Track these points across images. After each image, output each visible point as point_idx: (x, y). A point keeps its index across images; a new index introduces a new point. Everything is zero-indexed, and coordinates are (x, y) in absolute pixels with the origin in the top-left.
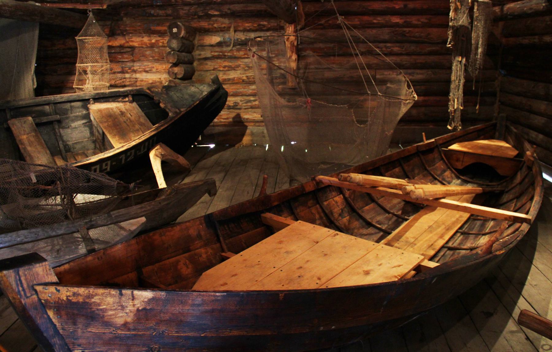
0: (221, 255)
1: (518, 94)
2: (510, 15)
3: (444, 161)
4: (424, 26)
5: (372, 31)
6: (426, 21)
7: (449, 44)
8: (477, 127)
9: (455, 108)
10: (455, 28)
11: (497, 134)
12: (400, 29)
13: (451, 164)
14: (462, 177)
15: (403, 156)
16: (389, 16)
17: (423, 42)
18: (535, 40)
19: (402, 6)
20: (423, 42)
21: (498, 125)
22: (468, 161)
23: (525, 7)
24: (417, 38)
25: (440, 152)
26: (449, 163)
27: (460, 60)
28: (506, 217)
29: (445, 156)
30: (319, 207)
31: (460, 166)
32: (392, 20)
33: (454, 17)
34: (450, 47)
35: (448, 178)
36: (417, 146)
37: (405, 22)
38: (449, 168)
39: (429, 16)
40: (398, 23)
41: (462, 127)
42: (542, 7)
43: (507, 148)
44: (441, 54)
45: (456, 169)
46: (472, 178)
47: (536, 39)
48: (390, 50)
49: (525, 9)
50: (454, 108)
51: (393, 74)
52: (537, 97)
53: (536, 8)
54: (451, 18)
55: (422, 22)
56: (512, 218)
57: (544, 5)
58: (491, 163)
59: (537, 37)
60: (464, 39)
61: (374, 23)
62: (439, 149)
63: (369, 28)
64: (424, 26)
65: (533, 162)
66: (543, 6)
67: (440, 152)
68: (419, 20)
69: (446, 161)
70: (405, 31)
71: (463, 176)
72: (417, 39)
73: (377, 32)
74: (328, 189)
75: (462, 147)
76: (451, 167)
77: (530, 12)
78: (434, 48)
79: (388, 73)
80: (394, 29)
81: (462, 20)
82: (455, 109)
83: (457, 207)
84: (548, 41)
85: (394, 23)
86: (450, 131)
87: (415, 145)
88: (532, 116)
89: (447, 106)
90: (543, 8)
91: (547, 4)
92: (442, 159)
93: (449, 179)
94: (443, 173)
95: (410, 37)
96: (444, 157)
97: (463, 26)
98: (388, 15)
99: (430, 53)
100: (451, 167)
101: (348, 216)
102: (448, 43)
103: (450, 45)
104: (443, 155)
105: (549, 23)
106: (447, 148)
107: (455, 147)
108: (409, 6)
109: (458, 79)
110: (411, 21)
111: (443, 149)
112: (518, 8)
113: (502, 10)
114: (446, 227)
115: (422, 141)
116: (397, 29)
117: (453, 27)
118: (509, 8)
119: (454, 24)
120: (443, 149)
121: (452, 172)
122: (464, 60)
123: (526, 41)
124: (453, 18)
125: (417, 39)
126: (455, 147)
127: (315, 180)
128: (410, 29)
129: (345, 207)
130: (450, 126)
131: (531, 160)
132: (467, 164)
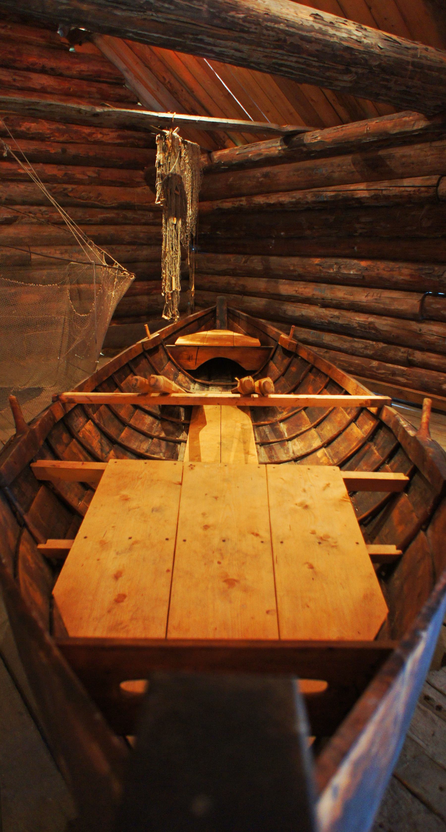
0: (40, 550)
1: (224, 273)
2: (224, 165)
3: (173, 362)
4: (92, 182)
5: (18, 187)
6: (94, 175)
7: (159, 200)
8: (198, 315)
9: (174, 289)
10: (166, 177)
11: (218, 322)
12: (60, 186)
13: (181, 366)
14: (200, 381)
15: (131, 359)
16: (41, 164)
17: (93, 206)
18: (241, 203)
19: (60, 150)
20: (93, 206)
21: (218, 311)
22: (204, 358)
23: (249, 152)
24: (84, 200)
25: (165, 350)
26: (179, 364)
27: (175, 223)
28: (362, 402)
29: (172, 354)
30: (76, 443)
31: (193, 366)
32: (46, 171)
33: (163, 161)
34: (159, 204)
35: (184, 383)
36: (142, 343)
37: (66, 174)
38: (180, 370)
39: (97, 169)
40: (55, 176)
41: (180, 316)
42: (277, 152)
43: (241, 336)
44: (116, 224)
45: (189, 371)
46: (209, 380)
47: (243, 201)
48: (48, 216)
49: (250, 155)
50: (171, 289)
51: (56, 253)
52: (251, 274)
53: (266, 153)
54: (159, 163)
55: (89, 176)
56: (369, 402)
57: (280, 148)
58: (233, 356)
59: (243, 199)
60: (178, 193)
61: (20, 174)
62: (163, 346)
63: (12, 181)
64: (92, 182)
65: (297, 346)
66: (279, 150)
67: (165, 350)
68: (84, 173)
69: (175, 362)
70: (65, 189)
71: (198, 378)
72: (84, 201)
73: (25, 188)
74: (74, 415)
75: (188, 340)
76: (182, 369)
77: (257, 159)
78: (108, 215)
79: (49, 252)
80: (50, 185)
81: (174, 167)
82: (173, 291)
83: (297, 401)
84: (262, 203)
85: (50, 175)
86: (167, 323)
87: (140, 342)
88: (246, 298)
89: (159, 288)
90: (279, 153)
91: (285, 147)
92: (169, 359)
93: (186, 384)
94: (176, 378)
95: (75, 197)
96: (171, 357)
97: (175, 175)
98: (38, 163)
99: (104, 222)
100: (182, 369)
101: (110, 450)
102: (157, 199)
103: (159, 202)
104: (169, 354)
105: (261, 180)
106: (174, 344)
107: (180, 341)
108: (68, 150)
109: (174, 250)
110: (74, 175)
111: (167, 346)
112: (238, 154)
113: (210, 158)
114: (239, 440)
115: (145, 335)
116: (55, 185)
117: (162, 176)
118: (221, 156)
119: (163, 172)
120: (167, 346)
121: (185, 375)
122: (180, 222)
123: (227, 205)
124: (161, 163)
125: (84, 201)
126: (180, 341)
127: (61, 400)
128: (74, 186)
129: (101, 438)
130: (166, 315)
131: (293, 344)
132: (203, 362)
